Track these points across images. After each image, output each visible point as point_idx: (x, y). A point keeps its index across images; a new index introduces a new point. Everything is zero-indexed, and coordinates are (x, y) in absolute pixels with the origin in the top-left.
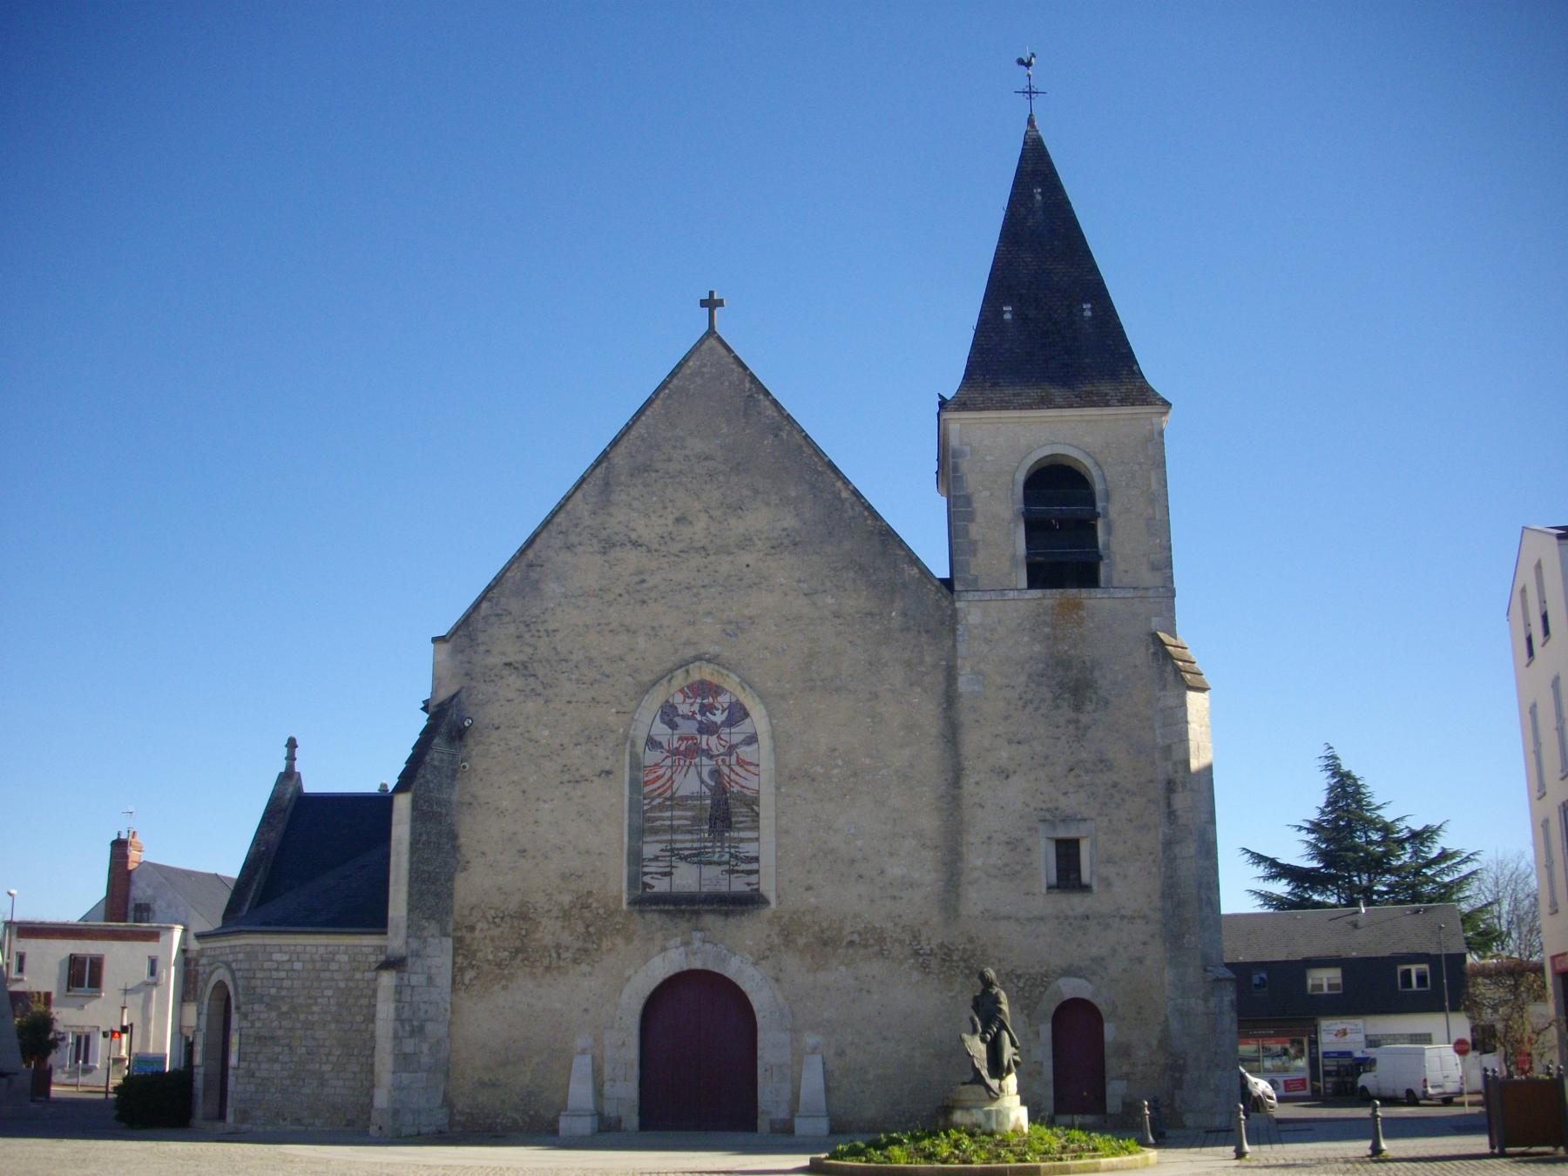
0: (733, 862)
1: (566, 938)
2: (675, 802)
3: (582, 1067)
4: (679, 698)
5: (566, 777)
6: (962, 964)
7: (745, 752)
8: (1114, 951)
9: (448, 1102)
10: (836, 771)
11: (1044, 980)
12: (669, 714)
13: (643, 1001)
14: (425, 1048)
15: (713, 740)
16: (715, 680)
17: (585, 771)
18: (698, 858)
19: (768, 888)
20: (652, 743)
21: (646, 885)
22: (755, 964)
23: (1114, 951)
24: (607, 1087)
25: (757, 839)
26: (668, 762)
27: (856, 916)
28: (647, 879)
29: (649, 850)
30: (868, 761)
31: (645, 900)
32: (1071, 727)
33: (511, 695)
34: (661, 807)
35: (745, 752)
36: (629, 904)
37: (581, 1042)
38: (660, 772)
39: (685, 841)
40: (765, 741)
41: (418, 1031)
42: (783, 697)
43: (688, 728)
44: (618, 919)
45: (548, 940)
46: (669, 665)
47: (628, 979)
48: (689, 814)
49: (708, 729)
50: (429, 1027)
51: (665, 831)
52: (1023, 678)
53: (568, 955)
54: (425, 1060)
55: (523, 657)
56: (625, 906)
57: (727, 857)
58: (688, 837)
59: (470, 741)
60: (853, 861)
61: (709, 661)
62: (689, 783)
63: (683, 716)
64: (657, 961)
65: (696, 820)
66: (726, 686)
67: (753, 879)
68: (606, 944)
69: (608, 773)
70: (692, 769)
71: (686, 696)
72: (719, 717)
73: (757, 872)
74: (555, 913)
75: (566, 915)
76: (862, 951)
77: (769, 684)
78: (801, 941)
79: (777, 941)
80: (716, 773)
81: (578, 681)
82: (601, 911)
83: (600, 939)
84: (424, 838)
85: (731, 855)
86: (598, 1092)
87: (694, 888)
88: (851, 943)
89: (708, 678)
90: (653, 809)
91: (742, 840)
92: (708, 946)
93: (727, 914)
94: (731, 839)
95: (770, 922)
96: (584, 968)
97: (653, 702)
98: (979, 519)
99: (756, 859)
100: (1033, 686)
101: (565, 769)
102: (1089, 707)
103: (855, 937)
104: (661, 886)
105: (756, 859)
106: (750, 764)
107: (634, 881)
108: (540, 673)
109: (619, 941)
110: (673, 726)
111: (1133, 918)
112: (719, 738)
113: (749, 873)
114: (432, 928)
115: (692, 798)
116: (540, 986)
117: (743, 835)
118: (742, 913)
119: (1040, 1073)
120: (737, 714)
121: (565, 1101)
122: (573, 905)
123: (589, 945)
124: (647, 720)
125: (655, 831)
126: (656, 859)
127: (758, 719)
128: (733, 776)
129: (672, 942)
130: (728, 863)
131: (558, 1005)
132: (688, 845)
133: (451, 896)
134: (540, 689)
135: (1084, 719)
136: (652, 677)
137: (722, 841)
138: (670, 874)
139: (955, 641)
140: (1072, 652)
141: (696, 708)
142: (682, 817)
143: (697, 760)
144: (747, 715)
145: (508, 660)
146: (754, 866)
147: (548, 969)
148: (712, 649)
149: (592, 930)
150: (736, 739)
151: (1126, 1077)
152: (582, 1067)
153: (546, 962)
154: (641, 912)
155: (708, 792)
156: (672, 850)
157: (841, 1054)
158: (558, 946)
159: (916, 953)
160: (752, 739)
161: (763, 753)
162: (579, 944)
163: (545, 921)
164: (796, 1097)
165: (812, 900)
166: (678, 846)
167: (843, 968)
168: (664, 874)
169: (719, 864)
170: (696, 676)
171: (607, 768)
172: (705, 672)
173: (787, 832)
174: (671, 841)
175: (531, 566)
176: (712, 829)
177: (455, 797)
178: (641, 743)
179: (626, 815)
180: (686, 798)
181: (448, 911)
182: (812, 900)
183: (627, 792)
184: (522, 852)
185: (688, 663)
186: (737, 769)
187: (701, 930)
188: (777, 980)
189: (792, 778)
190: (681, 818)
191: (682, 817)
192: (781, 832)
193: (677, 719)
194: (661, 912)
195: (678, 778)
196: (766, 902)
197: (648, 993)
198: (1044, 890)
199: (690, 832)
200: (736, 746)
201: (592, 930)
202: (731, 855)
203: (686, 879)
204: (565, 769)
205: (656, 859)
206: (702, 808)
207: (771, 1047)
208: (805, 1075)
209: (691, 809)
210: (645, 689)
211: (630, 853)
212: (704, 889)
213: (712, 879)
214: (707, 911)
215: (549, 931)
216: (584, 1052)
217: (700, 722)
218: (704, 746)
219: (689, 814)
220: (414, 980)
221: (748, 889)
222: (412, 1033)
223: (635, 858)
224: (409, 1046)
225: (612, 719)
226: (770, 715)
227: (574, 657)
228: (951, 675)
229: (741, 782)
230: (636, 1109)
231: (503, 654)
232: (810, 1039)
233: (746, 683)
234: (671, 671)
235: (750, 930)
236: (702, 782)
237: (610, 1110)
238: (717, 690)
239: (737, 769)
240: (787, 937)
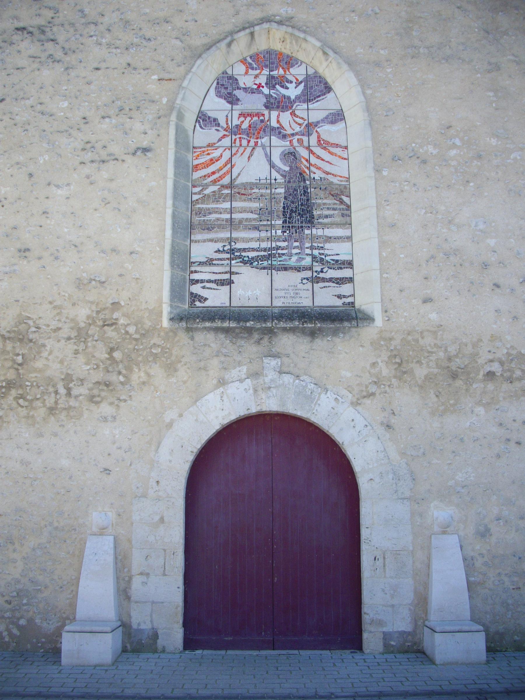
0: (317, 267)
1: (80, 367)
2: (235, 190)
3: (99, 554)
4: (239, 69)
5: (89, 156)
7: (328, 131)
10: (453, 153)
12: (227, 88)
13: (191, 458)
15: (286, 118)
16: (286, 49)
17: (115, 149)
18: (268, 261)
19: (367, 297)
20: (204, 119)
21: (195, 297)
22: (355, 404)
24: (137, 583)
25: (349, 238)
26: (227, 142)
27: (493, 338)
28: (196, 289)
29: (201, 251)
30: (494, 142)
31: (194, 316)
33: (22, 62)
34: (217, 197)
35: (328, 131)
37: (97, 518)
38: (216, 154)
39: (249, 240)
40: (356, 117)
42: (377, 64)
43: (254, 103)
44: (155, 340)
45: (55, 370)
46: (229, 27)
47: (170, 425)
48: (255, 205)
49: (282, 104)
51: (221, 227)
53: (82, 390)
55: (41, 21)
56: (165, 323)
57: (308, 261)
58: (255, 234)
60: (485, 266)
61: (280, 23)
62: (254, 167)
63: (245, 89)
64: (212, 399)
65: (265, 213)
66: (300, 56)
67: (346, 289)
68: (138, 376)
69: (145, 150)
70: (259, 151)
71: (249, 67)
72: (293, 92)
73: (351, 280)
74: (65, 332)
75: (81, 335)
76: (506, 386)
77: (359, 50)
78: (421, 372)
79: (385, 372)
80: (290, 156)
81: (109, 45)
82: (132, 329)
83: (129, 369)
85: (314, 258)
86: (124, 593)
87: (264, 301)
88: (490, 375)
89: (278, 46)
90: (205, 199)
91: (329, 239)
92: (287, 379)
93: (313, 334)
94: (313, 238)
95: (375, 345)
96: (106, 409)
97: (209, 69)
99: (350, 264)
101: (88, 146)
103: (496, 367)
104: (216, 298)
105: (350, 264)
106: (337, 146)
107: (177, 291)
108: (61, 39)
109: (157, 370)
110: (232, 100)
112: (293, 114)
113: (340, 281)
115: (256, 185)
116: (41, 435)
117: (329, 232)
118: (335, 333)
120: (317, 87)
121: (73, 605)
122: (91, 321)
123: (114, 378)
124: (198, 92)
125: (208, 227)
126: (210, 262)
127: (346, 92)
128: (313, 160)
129: (235, 373)
130: (310, 268)
131: (65, 463)
132: (255, 245)
134: (59, 54)
136: (206, 40)
137: (301, 240)
138: (230, 282)
141: (262, 80)
142: (245, 209)
143: (265, 140)
144: (328, 89)
145: (21, 25)
146: (346, 273)
147: (52, 410)
148: (284, 11)
149: (117, 355)
150: (315, 116)
152: (99, 554)
153: (50, 401)
154: (188, 330)
155: (280, 180)
156: (232, 251)
157: (484, 533)
158: (68, 379)
160: (337, 117)
161: (355, 133)
162: (99, 376)
163: (50, 344)
164: (422, 600)
165: (433, 316)
166: (239, 245)
167: (480, 410)
168: (221, 283)
169: (298, 269)
170: (262, 44)
171: (145, 144)
172: (272, 39)
173: (393, 226)
174: (230, 240)
176: (287, 225)
178: (190, 119)
179: (170, 202)
180: (252, 185)
182: (433, 316)
184: (24, 252)
185: (252, 25)
186: (318, 151)
187: (275, 356)
188: (389, 426)
189: (395, 159)
190: (243, 210)
191: (245, 209)
192: (386, 226)
193: (237, 93)
194: (217, 330)
195: (239, 161)
196: (368, 319)
197: (198, 446)
199: (256, 228)
200: (316, 124)
201: (117, 355)
202: (314, 258)
203: (252, 289)
204: (88, 146)
205: (210, 262)
206: (272, 198)
207: (383, 526)
208: (436, 565)
209: (258, 199)
210: (198, 54)
211: (174, 252)
212: (278, 303)
213: (289, 290)
214: (285, 329)
215: (56, 358)
216: (102, 532)
217: (268, 97)
218: (274, 124)
219: (255, 205)
221: (339, 302)
223: (181, 260)
225: (153, 87)
226: (363, 84)
227: (106, 20)
229: (326, 167)
230: (180, 619)
231: (16, 18)
232: (440, 512)
233: (328, 49)
234: (231, 33)
235: (345, 357)
236: (272, 166)
237: (141, 619)
238: (289, 62)
239: (318, 151)
240: (401, 366)
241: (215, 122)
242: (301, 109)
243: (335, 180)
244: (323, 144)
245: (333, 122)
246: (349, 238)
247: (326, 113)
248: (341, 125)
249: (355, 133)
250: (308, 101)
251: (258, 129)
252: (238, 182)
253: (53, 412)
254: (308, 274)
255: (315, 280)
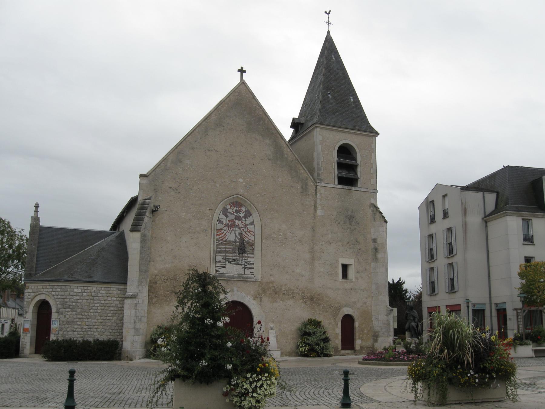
2: (227, 243)
7: (250, 227)
20: (219, 221)
22: (254, 299)
26: (225, 228)
27: (285, 285)
34: (222, 244)
35: (250, 227)
38: (222, 232)
39: (230, 256)
43: (232, 217)
49: (238, 218)
51: (223, 252)
58: (231, 255)
62: (232, 236)
65: (234, 249)
67: (252, 271)
71: (231, 206)
72: (242, 215)
73: (253, 268)
76: (287, 297)
80: (240, 234)
88: (284, 294)
90: (219, 244)
91: (249, 257)
94: (245, 257)
103: (285, 292)
105: (253, 264)
113: (251, 268)
117: (249, 255)
124: (218, 214)
125: (220, 252)
126: (220, 262)
132: (231, 258)
138: (225, 267)
141: (234, 211)
142: (229, 248)
143: (234, 229)
144: (251, 215)
150: (247, 223)
160: (252, 223)
167: (281, 302)
168: (223, 267)
169: (241, 265)
186: (247, 233)
190: (229, 248)
191: (229, 248)
199: (232, 253)
205: (220, 262)
206: (236, 245)
209: (232, 245)
229: (250, 238)
236: (236, 236)
239: (247, 233)
241: (222, 222)
242: (244, 220)
243: (251, 241)
244: (249, 231)
245: (251, 225)
246: (254, 257)
247: (166, 374)
248: (253, 226)
249: (256, 228)
250: (246, 218)
251: (233, 226)
252: (228, 240)
253: (241, 251)
254: (243, 266)
255: (246, 268)
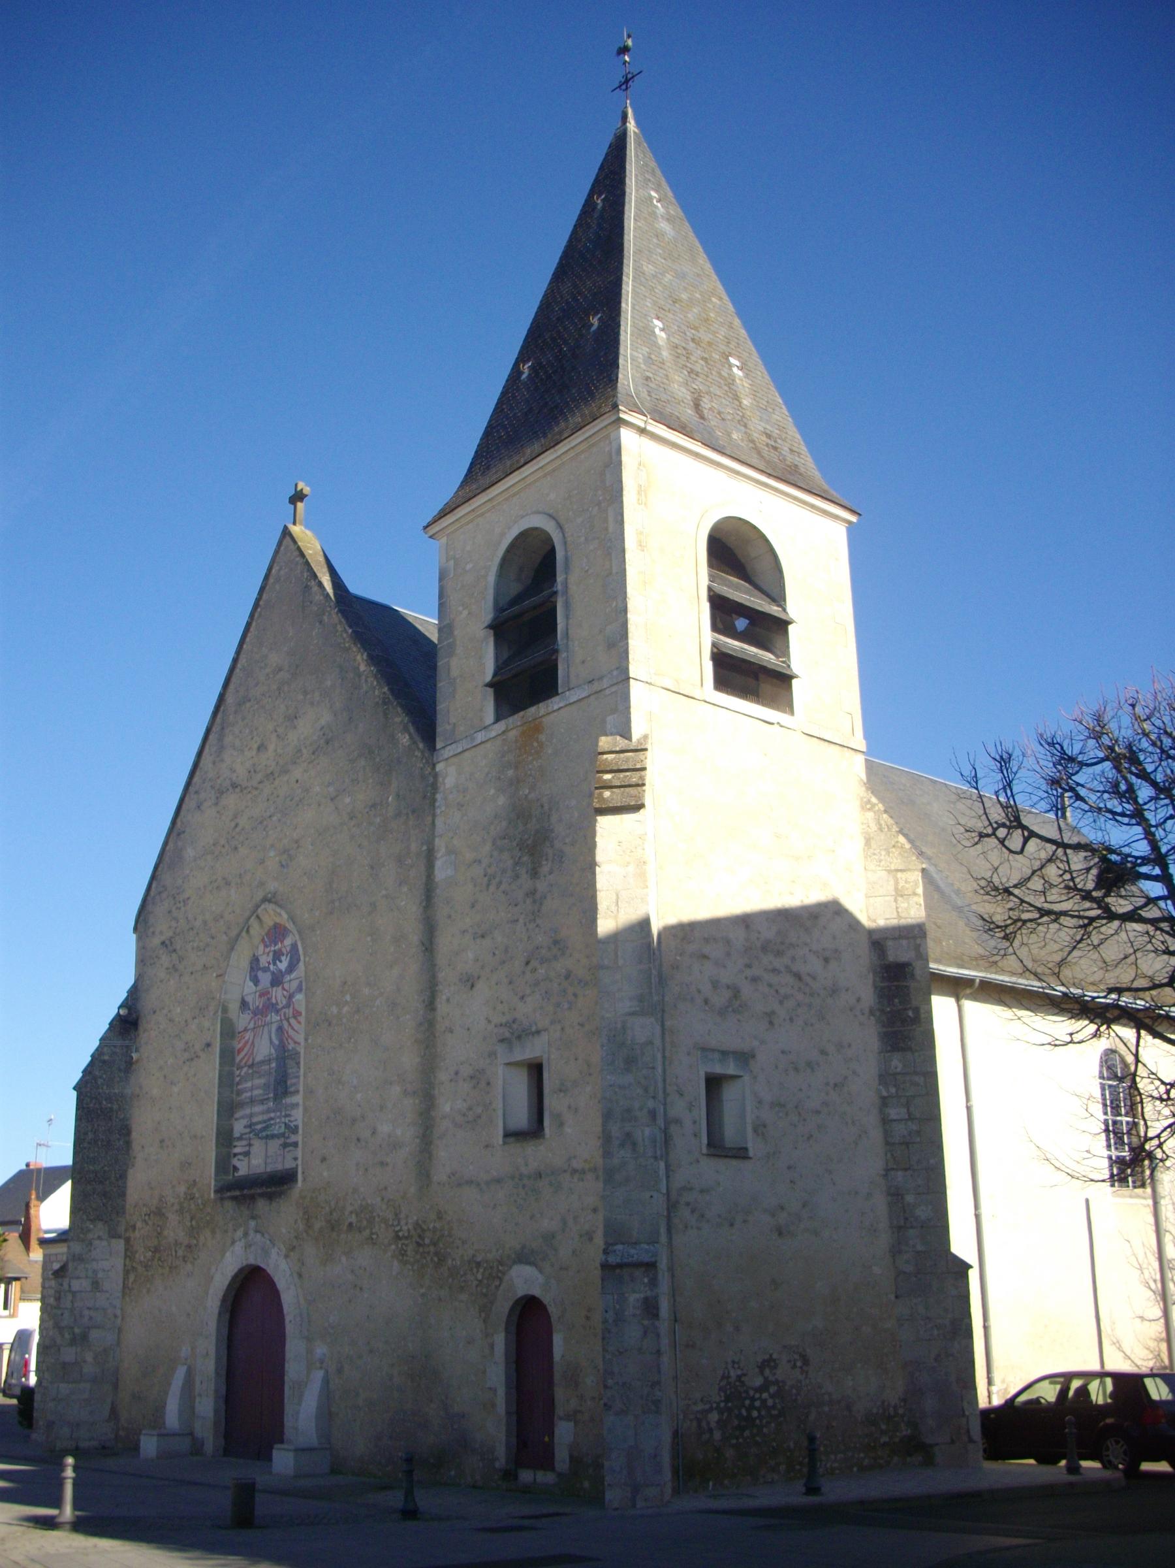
6: (432, 1249)
8: (564, 1222)
9: (114, 1413)
11: (495, 1272)
14: (89, 1357)
23: (564, 1222)
32: (529, 901)
36: (216, 1192)
41: (81, 1340)
50: (94, 1334)
52: (488, 847)
54: (87, 1369)
56: (212, 1195)
59: (141, 1029)
84: (90, 1136)
98: (459, 650)
100: (495, 853)
102: (545, 869)
107: (224, 1164)
111: (583, 1172)
112: (284, 989)
114: (100, 1229)
119: (494, 1405)
130: (283, 1135)
133: (123, 1195)
135: (541, 886)
139: (434, 816)
140: (532, 796)
151: (572, 1416)
159: (397, 1237)
175: (179, 834)
177: (128, 1091)
178: (234, 1007)
181: (120, 1211)
183: (217, 1066)
198: (499, 1139)
211: (218, 1134)
212: (268, 1170)
220: (76, 1285)
222: (73, 1342)
223: (885, 1121)
224: (69, 1354)
228: (430, 858)
